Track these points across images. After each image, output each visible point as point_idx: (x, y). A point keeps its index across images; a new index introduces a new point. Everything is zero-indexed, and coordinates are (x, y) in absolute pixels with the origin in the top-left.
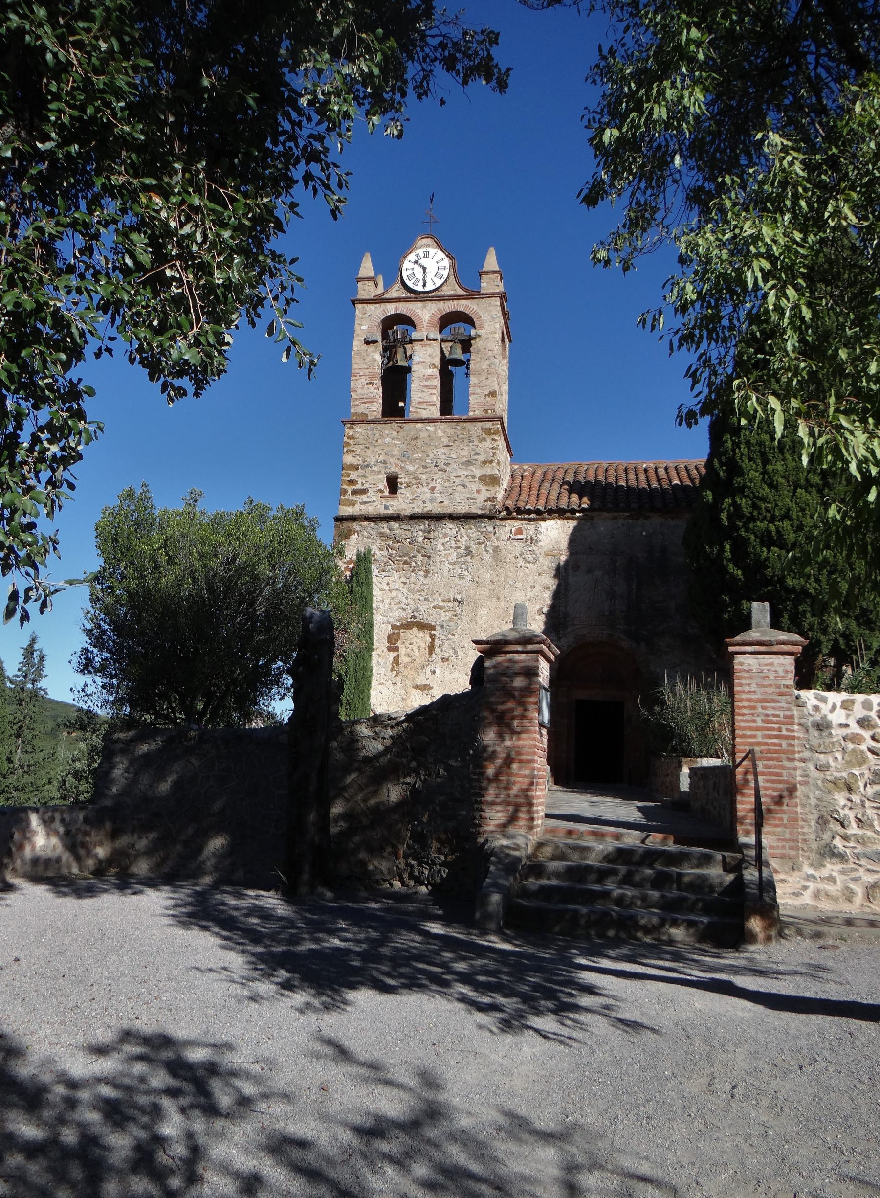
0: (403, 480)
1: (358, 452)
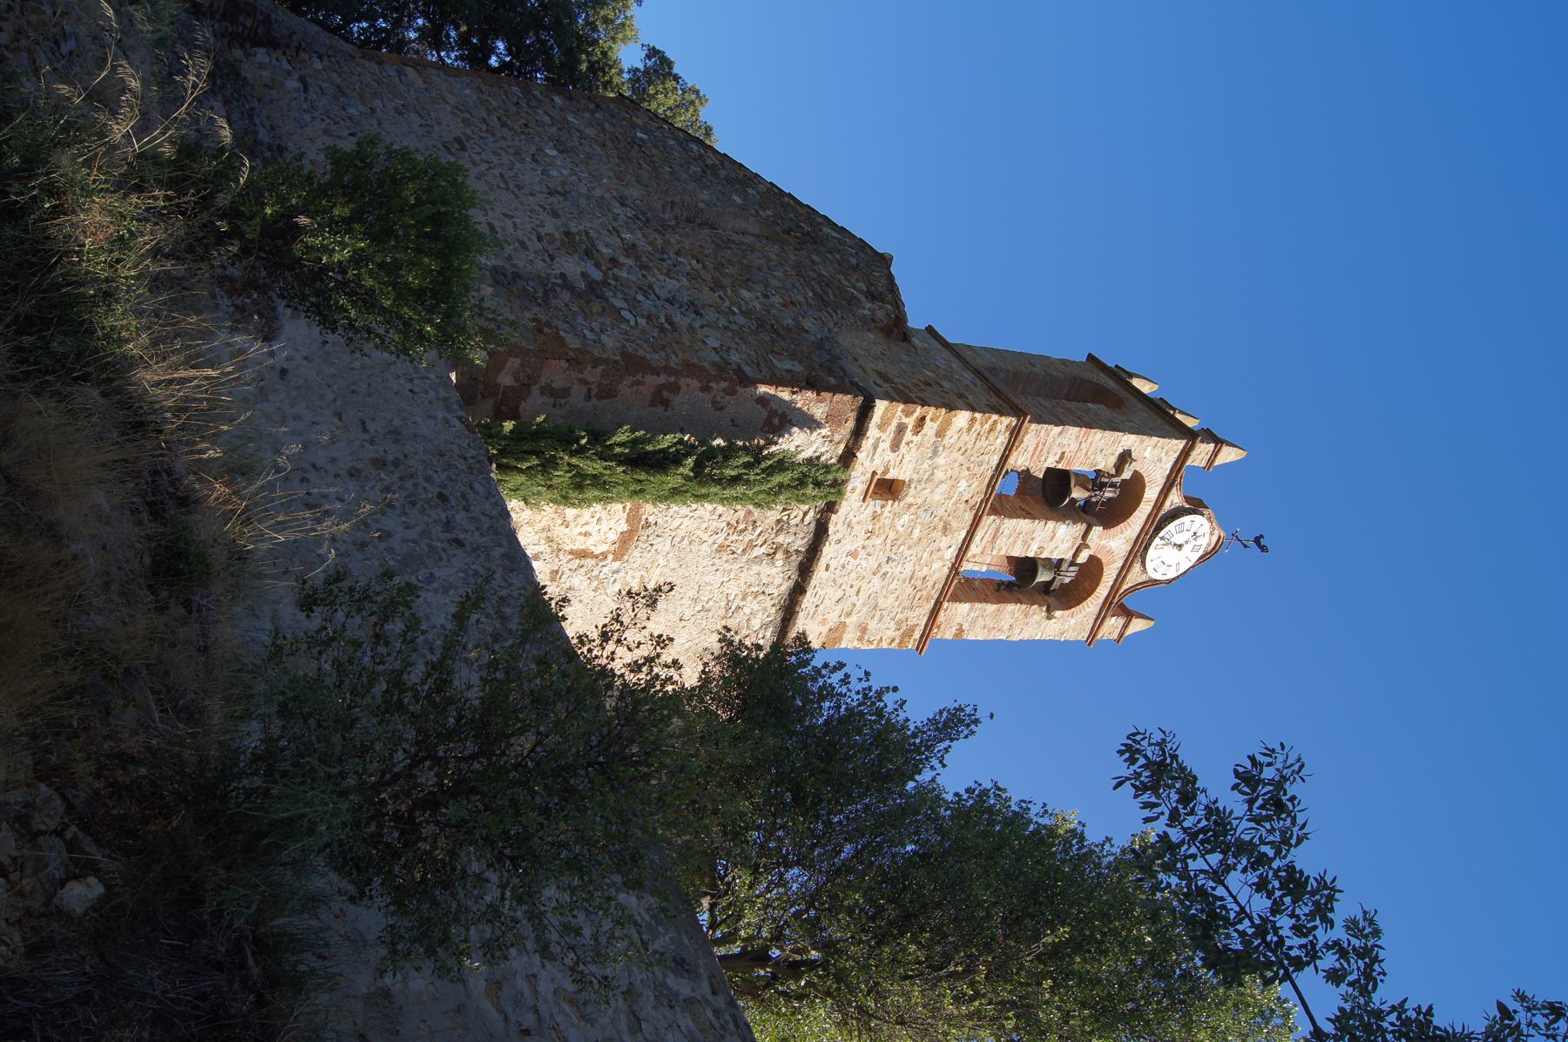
0: (888, 508)
1: (965, 437)
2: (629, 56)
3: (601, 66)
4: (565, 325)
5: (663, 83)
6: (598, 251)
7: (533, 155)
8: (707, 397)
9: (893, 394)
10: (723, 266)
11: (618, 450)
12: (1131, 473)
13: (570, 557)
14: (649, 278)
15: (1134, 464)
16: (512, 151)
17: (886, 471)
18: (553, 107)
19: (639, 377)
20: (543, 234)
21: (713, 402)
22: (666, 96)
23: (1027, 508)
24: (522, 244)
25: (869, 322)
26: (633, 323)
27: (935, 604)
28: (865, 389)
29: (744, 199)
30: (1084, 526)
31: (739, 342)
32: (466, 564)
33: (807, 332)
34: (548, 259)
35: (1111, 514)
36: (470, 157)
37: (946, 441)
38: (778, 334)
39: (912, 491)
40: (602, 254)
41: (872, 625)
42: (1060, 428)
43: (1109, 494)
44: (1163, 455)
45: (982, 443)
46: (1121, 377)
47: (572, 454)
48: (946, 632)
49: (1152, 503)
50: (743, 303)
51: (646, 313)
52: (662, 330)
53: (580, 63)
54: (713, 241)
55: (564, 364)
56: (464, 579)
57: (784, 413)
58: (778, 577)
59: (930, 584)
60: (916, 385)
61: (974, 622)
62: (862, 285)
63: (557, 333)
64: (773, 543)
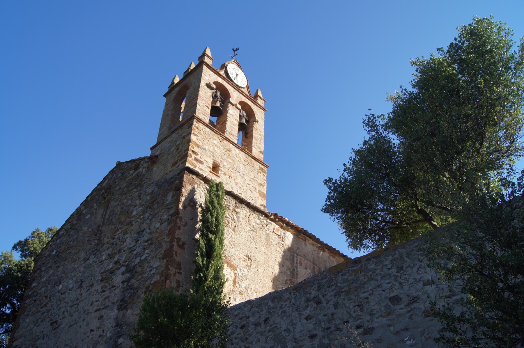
0: (222, 169)
1: (199, 138)
2: (16, 257)
3: (20, 267)
4: (148, 281)
5: (30, 244)
6: (111, 269)
7: (61, 294)
8: (182, 228)
9: (183, 161)
10: (120, 222)
11: (205, 262)
12: (214, 85)
13: (235, 287)
14: (125, 249)
15: (211, 83)
16: (59, 303)
17: (210, 167)
18: (38, 286)
19: (174, 253)
20: (101, 290)
21: (184, 226)
22: (35, 244)
23: (222, 123)
24: (106, 298)
25: (149, 169)
26: (147, 255)
27: (253, 158)
28: (181, 170)
29: (88, 214)
30: (230, 105)
31: (157, 216)
32: (279, 316)
33: (153, 191)
34: (114, 288)
35: (225, 96)
36: (61, 319)
37: (201, 144)
38: (154, 201)
39: (217, 160)
40: (112, 267)
41: (259, 181)
42: (198, 105)
43: (218, 94)
44: (208, 73)
45: (202, 132)
46: (172, 87)
47: (206, 280)
48: (261, 157)
49: (223, 80)
50: (139, 214)
51: (143, 250)
52: (151, 244)
53: (18, 275)
54: (108, 225)
55: (168, 281)
56: (287, 317)
57: (189, 200)
58: (244, 211)
59: (246, 159)
60: (179, 153)
61: (258, 147)
62: (131, 172)
63: (152, 284)
64: (233, 211)
